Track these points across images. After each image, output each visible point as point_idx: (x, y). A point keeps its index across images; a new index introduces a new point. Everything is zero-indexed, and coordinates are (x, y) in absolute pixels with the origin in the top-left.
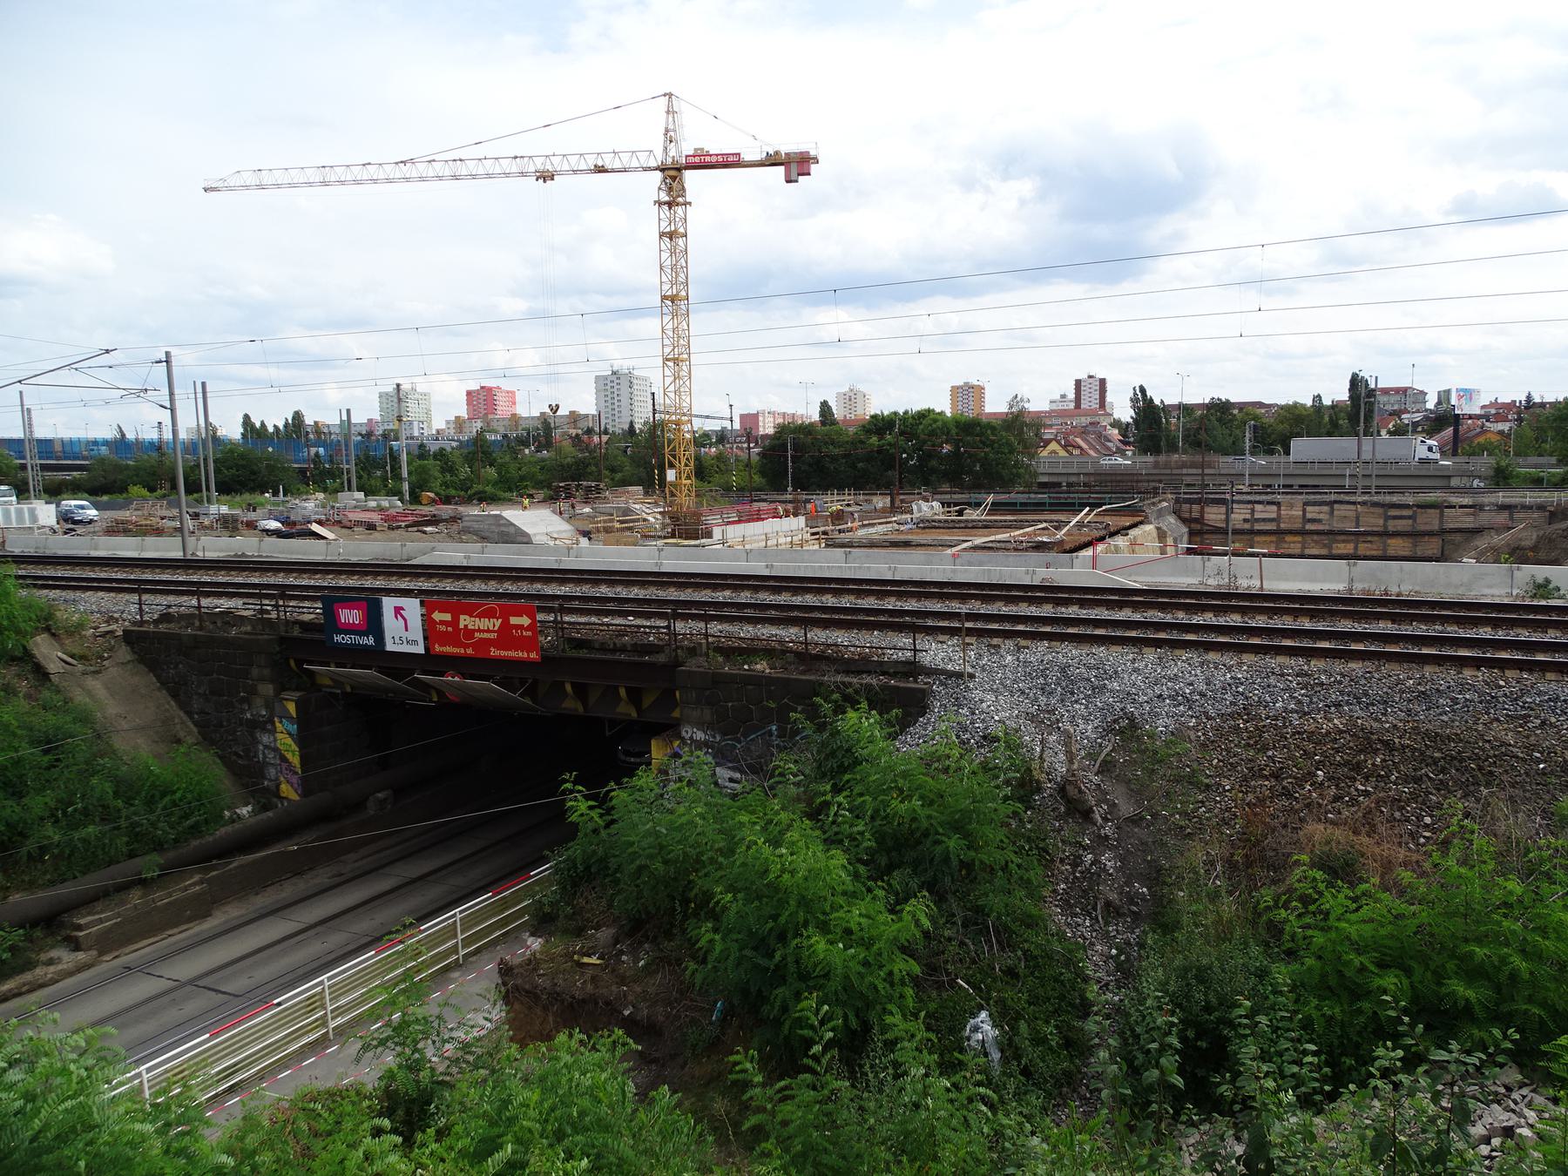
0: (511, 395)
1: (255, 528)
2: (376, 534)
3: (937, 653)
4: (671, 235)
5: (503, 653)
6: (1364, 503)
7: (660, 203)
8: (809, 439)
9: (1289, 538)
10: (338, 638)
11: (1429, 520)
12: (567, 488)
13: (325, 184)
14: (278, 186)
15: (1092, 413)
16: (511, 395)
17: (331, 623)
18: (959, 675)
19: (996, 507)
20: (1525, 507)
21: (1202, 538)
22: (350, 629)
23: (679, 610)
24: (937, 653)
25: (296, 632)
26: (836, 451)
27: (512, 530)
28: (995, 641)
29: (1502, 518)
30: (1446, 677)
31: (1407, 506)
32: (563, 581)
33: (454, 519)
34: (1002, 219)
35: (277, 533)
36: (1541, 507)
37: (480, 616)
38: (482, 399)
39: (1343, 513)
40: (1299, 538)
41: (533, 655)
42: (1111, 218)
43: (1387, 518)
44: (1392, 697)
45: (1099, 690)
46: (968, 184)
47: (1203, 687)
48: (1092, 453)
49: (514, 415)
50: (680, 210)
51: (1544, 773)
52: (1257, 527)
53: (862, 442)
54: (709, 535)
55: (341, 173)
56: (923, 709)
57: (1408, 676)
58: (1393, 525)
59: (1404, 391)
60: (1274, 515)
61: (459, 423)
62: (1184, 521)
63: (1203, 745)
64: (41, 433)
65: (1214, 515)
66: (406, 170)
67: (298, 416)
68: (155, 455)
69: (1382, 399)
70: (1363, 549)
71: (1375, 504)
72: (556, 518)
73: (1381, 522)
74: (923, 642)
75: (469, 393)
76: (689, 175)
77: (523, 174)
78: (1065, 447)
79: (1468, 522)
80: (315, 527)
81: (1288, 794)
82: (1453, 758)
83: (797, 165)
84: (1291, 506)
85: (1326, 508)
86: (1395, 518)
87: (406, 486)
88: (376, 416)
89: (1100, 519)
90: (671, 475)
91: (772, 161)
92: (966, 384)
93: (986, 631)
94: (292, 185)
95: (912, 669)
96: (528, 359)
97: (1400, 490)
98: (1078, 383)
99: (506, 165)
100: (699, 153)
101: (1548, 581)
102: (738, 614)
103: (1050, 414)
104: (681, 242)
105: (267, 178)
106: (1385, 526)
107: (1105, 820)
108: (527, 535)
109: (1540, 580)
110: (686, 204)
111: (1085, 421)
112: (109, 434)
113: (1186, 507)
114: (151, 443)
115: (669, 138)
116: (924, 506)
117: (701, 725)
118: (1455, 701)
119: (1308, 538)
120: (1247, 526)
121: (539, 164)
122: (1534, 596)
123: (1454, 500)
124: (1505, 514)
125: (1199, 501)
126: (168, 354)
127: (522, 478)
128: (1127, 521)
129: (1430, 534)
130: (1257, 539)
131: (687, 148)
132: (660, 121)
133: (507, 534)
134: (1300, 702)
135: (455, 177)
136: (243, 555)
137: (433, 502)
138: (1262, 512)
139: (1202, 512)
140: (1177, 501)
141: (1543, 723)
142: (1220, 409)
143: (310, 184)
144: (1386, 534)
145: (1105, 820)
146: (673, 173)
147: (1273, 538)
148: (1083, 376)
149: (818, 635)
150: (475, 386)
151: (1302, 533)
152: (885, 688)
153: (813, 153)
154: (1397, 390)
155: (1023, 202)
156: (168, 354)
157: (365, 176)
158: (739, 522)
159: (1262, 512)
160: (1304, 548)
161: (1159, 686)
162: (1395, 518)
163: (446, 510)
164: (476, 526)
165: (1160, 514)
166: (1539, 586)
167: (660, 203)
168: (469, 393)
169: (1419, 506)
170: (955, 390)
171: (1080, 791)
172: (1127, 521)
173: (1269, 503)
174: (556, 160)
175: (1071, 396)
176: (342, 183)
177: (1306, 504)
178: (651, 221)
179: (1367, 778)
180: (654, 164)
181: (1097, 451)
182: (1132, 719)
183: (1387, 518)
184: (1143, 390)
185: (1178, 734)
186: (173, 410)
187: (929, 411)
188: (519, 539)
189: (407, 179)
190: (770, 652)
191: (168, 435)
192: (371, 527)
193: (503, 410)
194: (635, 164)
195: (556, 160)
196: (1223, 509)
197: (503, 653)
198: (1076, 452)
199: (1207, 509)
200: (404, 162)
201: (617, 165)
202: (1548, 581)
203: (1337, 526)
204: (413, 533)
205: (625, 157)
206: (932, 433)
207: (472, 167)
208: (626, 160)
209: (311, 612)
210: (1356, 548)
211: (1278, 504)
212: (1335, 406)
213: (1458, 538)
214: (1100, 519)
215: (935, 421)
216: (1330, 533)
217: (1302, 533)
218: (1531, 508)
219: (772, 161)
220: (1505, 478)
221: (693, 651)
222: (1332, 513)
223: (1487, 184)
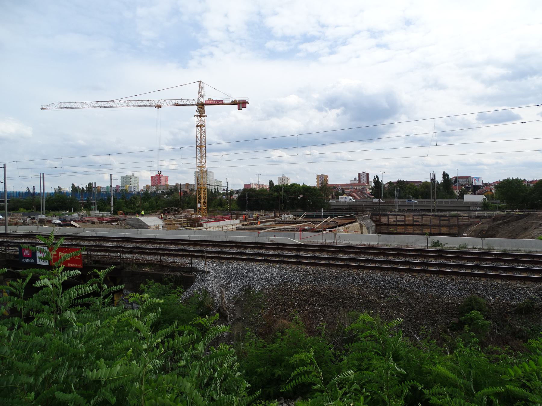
0: (166, 178)
1: (51, 223)
2: (95, 225)
3: (201, 264)
4: (200, 126)
5: (72, 265)
6: (432, 215)
7: (196, 116)
8: (254, 194)
9: (408, 227)
10: (23, 260)
11: (454, 221)
12: (168, 210)
13: (83, 108)
14: (67, 108)
15: (364, 185)
16: (166, 178)
17: (21, 255)
18: (205, 272)
19: (307, 217)
20: (485, 217)
21: (381, 229)
22: (26, 257)
23: (123, 251)
24: (201, 264)
25: (12, 258)
26: (263, 197)
27: (143, 224)
28: (223, 261)
29: (477, 220)
30: (345, 272)
31: (446, 216)
32: (108, 241)
33: (125, 220)
34: (331, 120)
35: (59, 225)
36: (490, 217)
37: (65, 253)
38: (157, 179)
39: (426, 219)
40: (412, 227)
41: (80, 266)
42: (368, 119)
43: (440, 220)
44: (327, 278)
45: (245, 276)
46: (320, 109)
47: (275, 276)
48: (359, 198)
49: (167, 184)
50: (203, 118)
51: (361, 303)
52: (398, 223)
53: (272, 194)
54: (202, 226)
55: (89, 104)
56: (192, 283)
57: (335, 272)
58: (442, 223)
59: (468, 177)
60: (403, 219)
61: (148, 186)
62: (374, 221)
63: (267, 295)
64: (8, 190)
65: (384, 219)
66: (111, 104)
67: (90, 184)
68: (32, 197)
69: (460, 180)
70: (433, 231)
71: (436, 216)
72: (159, 220)
73: (438, 222)
74: (195, 260)
75: (152, 177)
76: (206, 107)
77: (151, 106)
79: (467, 222)
80: (72, 223)
81: (285, 310)
82: (337, 298)
83: (242, 105)
84: (409, 216)
85: (420, 217)
86: (443, 220)
87: (112, 209)
89: (335, 220)
90: (199, 205)
91: (233, 103)
93: (219, 258)
94: (72, 108)
95: (192, 270)
96: (173, 166)
97: (445, 211)
98: (359, 174)
99: (145, 103)
100: (210, 100)
101: (438, 241)
102: (141, 251)
103: (349, 185)
104: (203, 128)
105: (63, 105)
106: (440, 223)
107: (231, 319)
108: (147, 225)
109: (436, 241)
110: (205, 116)
111: (361, 187)
112: (25, 190)
113: (374, 216)
114: (26, 192)
115: (200, 95)
116: (286, 216)
118: (345, 279)
119: (415, 227)
120: (395, 223)
121: (156, 102)
122: (433, 246)
123: (462, 214)
124: (479, 219)
125: (378, 215)
126: (4, 165)
127: (157, 206)
128: (347, 221)
129: (455, 226)
130: (398, 227)
131: (206, 99)
132: (197, 90)
133: (141, 225)
134: (301, 280)
135: (128, 106)
136: (32, 232)
137: (122, 214)
138: (400, 218)
139: (380, 218)
140: (372, 215)
141: (367, 287)
142: (401, 184)
143: (78, 108)
144: (440, 226)
145: (231, 319)
146: (201, 106)
147: (404, 227)
149: (164, 258)
150: (124, 175)
151: (413, 225)
152: (181, 276)
153: (247, 101)
154: (466, 177)
155: (338, 115)
156: (4, 165)
157: (98, 105)
158: (215, 221)
159: (400, 218)
160: (414, 230)
161: (261, 274)
162: (443, 220)
163: (123, 217)
164: (131, 222)
165: (364, 219)
166: (436, 243)
167: (196, 116)
168: (152, 177)
169: (450, 216)
170: (318, 177)
171: (224, 310)
172: (347, 221)
173: (402, 215)
174: (162, 102)
175: (358, 179)
176: (89, 107)
177: (414, 216)
178: (194, 120)
179: (309, 305)
180: (195, 103)
181: (360, 197)
182: (250, 286)
183: (440, 220)
184: (377, 177)
185: (261, 291)
186: (5, 183)
187: (295, 184)
188: (145, 227)
189: (112, 107)
190: (150, 264)
191: (38, 190)
192: (93, 222)
193: (163, 183)
194: (188, 103)
195: (162, 102)
196: (387, 218)
197: (72, 265)
199: (381, 217)
200: (111, 101)
201: (182, 103)
202: (438, 241)
203: (424, 223)
204: (109, 225)
205: (168, 101)
206: (295, 191)
207: (133, 103)
208: (185, 102)
209: (14, 250)
210: (431, 231)
211: (405, 216)
212: (441, 183)
213: (464, 227)
214: (335, 220)
215: (296, 187)
216: (422, 225)
217: (413, 225)
218: (486, 217)
219: (233, 103)
220: (487, 207)
221: (129, 264)
222: (422, 218)
223: (489, 109)
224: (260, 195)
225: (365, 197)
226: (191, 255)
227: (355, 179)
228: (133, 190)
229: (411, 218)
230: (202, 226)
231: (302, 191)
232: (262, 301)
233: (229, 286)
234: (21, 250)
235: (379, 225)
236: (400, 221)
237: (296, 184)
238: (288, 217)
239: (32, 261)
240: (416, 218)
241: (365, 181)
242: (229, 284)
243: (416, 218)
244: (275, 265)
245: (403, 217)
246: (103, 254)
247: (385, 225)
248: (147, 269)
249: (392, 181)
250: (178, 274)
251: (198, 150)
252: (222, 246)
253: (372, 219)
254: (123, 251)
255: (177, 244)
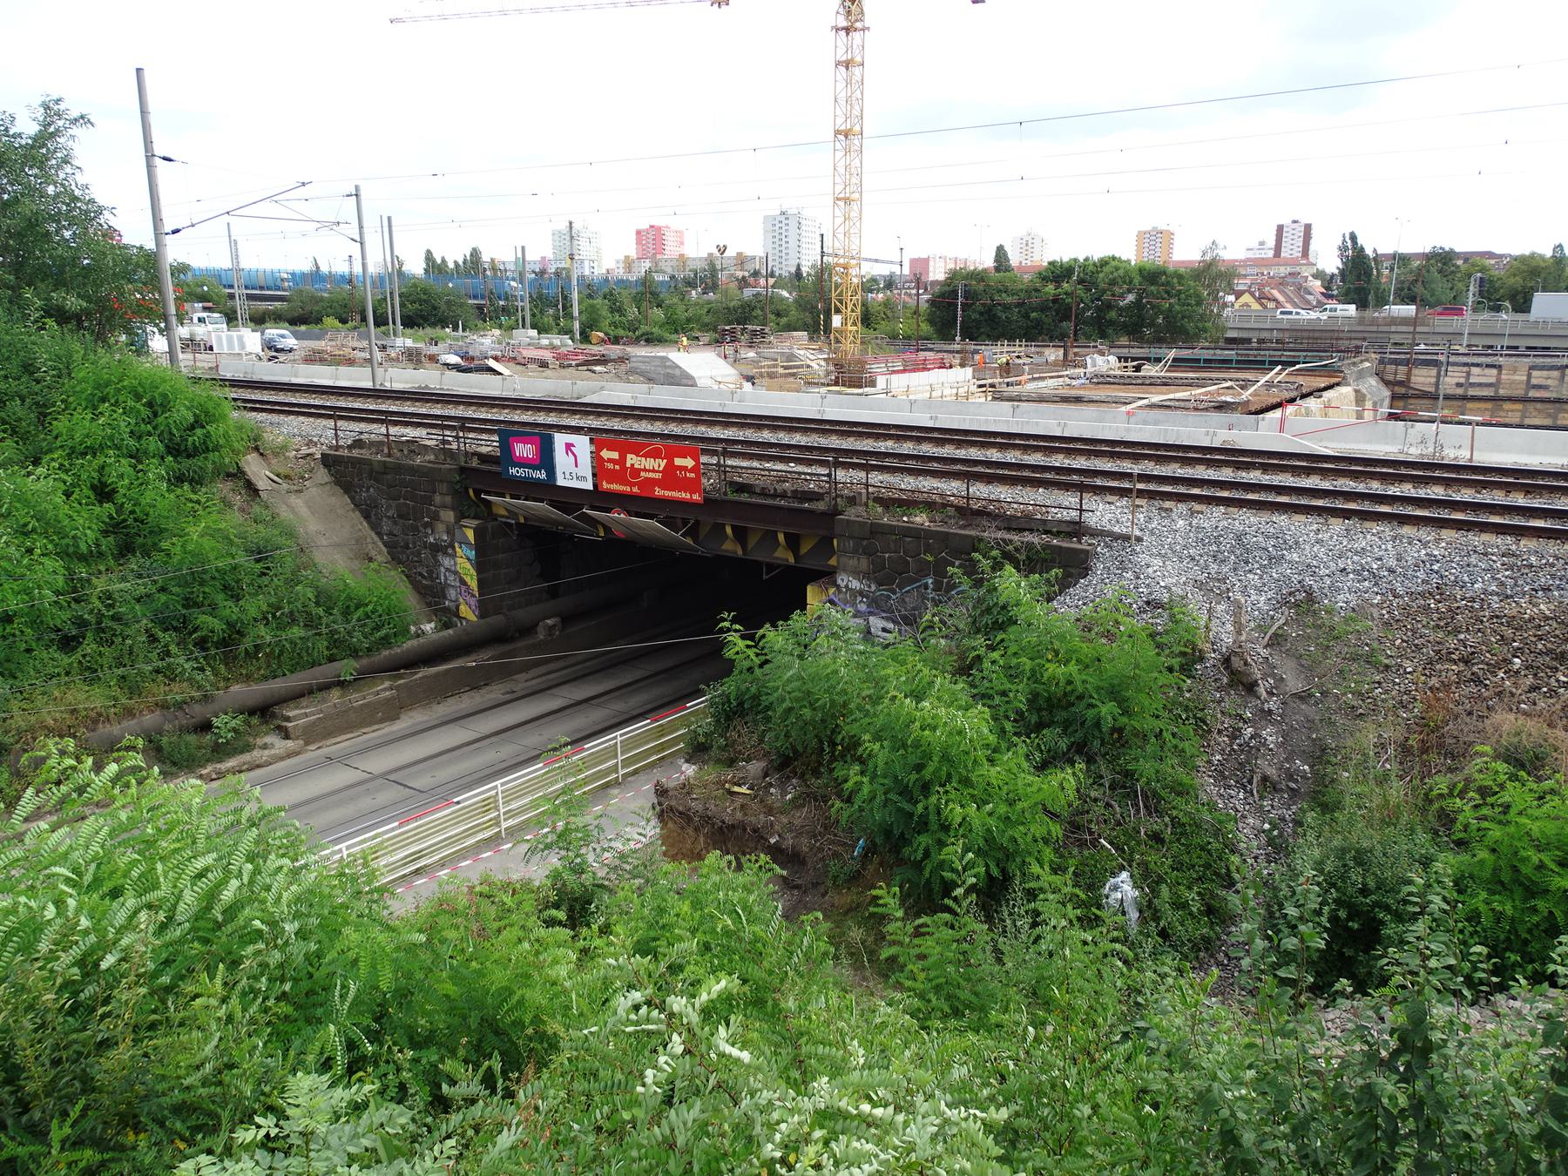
2: (548, 372)
3: (1103, 513)
4: (847, 64)
5: (667, 493)
8: (981, 287)
9: (1507, 406)
10: (513, 471)
12: (732, 332)
17: (506, 456)
23: (840, 459)
24: (1103, 513)
25: (475, 463)
27: (677, 372)
28: (1167, 504)
33: (622, 360)
37: (646, 456)
38: (651, 239)
40: (1519, 406)
41: (696, 497)
49: (682, 256)
50: (857, 36)
52: (1471, 392)
53: (1037, 290)
54: (872, 384)
56: (1085, 571)
60: (1493, 380)
62: (1387, 383)
63: (1387, 624)
65: (1423, 378)
67: (475, 253)
74: (1090, 501)
75: (638, 232)
78: (1258, 300)
84: (1515, 370)
85: (1556, 374)
87: (577, 325)
88: (550, 255)
89: (1292, 379)
92: (1154, 229)
93: (1157, 493)
95: (1076, 529)
98: (1280, 229)
107: (1271, 694)
108: (692, 378)
111: (1283, 271)
112: (305, 267)
116: (1099, 359)
117: (856, 573)
119: (1531, 407)
120: (1460, 391)
125: (1407, 363)
126: (357, 188)
128: (1322, 382)
133: (673, 376)
138: (1477, 375)
139: (1409, 374)
140: (1381, 361)
145: (1271, 694)
147: (1489, 405)
148: (1286, 221)
149: (980, 490)
151: (1525, 400)
156: (357, 188)
158: (904, 371)
159: (1477, 375)
160: (1523, 417)
163: (614, 351)
165: (1361, 375)
172: (1322, 382)
177: (1532, 368)
182: (1310, 593)
187: (1114, 258)
192: (544, 365)
193: (671, 251)
196: (1434, 372)
197: (667, 493)
198: (1271, 305)
199: (1415, 371)
206: (1113, 283)
211: (1499, 367)
214: (1292, 379)
215: (1117, 269)
221: (852, 501)
224: (999, 291)
225: (1308, 302)
226: (1084, 484)
227: (1262, 243)
228: (587, 273)
229: (1521, 377)
230: (872, 384)
231: (1136, 281)
232: (1375, 645)
233: (1223, 587)
234: (506, 446)
235: (1404, 397)
236: (1480, 385)
237: (1120, 260)
238: (1103, 362)
239: (541, 475)
240: (1538, 377)
241: (1297, 253)
242: (1223, 581)
243: (1538, 377)
244: (1376, 527)
245: (1494, 372)
246: (745, 464)
247: (1424, 395)
248: (921, 519)
249: (1405, 249)
250: (1029, 537)
251: (838, 146)
252: (1120, 456)
253: (1379, 374)
254: (840, 459)
255: (941, 442)
